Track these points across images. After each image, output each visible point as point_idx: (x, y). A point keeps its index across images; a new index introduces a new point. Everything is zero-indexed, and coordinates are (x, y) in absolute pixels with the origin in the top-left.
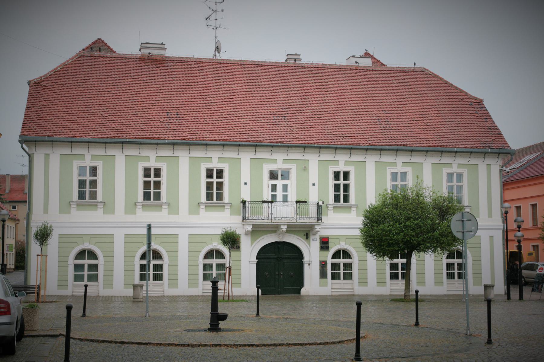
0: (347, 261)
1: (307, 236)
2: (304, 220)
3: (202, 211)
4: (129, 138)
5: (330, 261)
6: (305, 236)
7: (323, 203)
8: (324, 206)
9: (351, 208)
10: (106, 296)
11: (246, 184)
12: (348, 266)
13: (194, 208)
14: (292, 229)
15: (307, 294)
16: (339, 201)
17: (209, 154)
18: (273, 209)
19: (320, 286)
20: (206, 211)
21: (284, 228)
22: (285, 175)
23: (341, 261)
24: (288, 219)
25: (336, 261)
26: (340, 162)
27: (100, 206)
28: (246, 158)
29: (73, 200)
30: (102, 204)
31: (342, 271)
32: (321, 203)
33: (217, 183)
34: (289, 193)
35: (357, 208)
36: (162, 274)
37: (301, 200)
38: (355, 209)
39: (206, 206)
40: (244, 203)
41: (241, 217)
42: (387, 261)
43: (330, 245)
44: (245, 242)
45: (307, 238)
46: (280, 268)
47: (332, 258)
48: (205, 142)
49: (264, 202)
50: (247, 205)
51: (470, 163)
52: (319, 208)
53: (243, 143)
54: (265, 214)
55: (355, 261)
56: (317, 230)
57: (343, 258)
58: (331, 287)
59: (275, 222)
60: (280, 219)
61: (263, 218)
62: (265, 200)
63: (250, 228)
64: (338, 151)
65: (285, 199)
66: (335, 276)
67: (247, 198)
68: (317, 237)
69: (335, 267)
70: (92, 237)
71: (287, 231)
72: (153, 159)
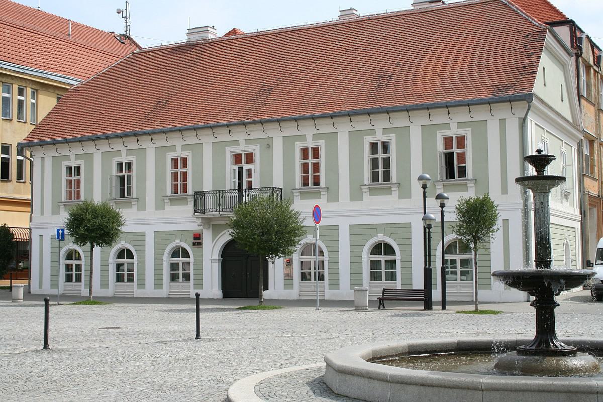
0: (390, 257)
3: (366, 196)
12: (392, 264)
13: (356, 195)
19: (284, 289)
26: (488, 121)
27: (324, 193)
29: (134, 197)
30: (396, 185)
33: (458, 154)
34: (252, 179)
36: (396, 271)
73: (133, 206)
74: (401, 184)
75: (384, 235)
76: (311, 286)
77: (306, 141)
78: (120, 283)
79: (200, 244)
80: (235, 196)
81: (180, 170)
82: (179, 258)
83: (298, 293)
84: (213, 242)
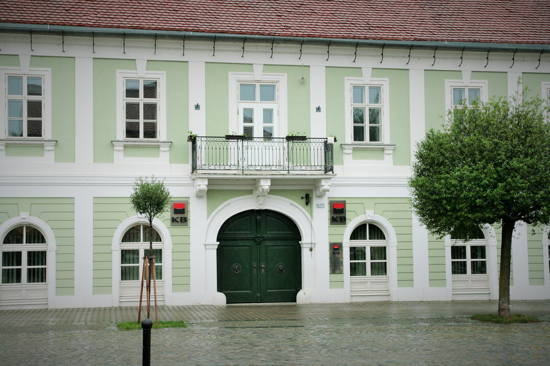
0: (36, 247)
1: (308, 199)
2: (300, 172)
3: (119, 155)
4: (51, 24)
5: (347, 244)
6: (304, 201)
7: (335, 140)
8: (336, 146)
9: (383, 150)
10: (105, 309)
11: (197, 107)
12: (38, 258)
14: (280, 187)
15: (308, 302)
16: (362, 139)
17: (249, 58)
18: (290, 151)
19: (331, 287)
20: (354, 158)
21: (266, 185)
22: (269, 92)
23: (367, 244)
24: (273, 168)
25: (358, 243)
27: (49, 147)
28: (198, 61)
31: (368, 261)
32: (331, 140)
33: (146, 106)
35: (393, 150)
37: (295, 134)
38: (391, 152)
39: (125, 147)
40: (193, 139)
41: (189, 166)
42: (448, 241)
43: (348, 215)
44: (197, 211)
45: (307, 204)
46: (259, 255)
47: (351, 239)
48: (244, 36)
49: (229, 137)
50: (198, 143)
51: (488, 69)
52: (328, 147)
53: (191, 33)
54: (233, 160)
55: (391, 243)
56: (324, 188)
57: (370, 238)
58: (348, 290)
59: (251, 174)
60: (258, 168)
61: (227, 168)
62: (231, 134)
63: (203, 185)
64: (360, 50)
65: (268, 136)
66: (355, 270)
67: (199, 130)
68: (325, 201)
69: (356, 253)
70: (33, 201)
71: (272, 192)
72: (141, 65)
73: (45, 152)
74: (59, 141)
75: (30, 215)
76: (366, 282)
77: (362, 76)
78: (358, 278)
79: (184, 221)
80: (319, 150)
81: (367, 105)
82: (140, 241)
83: (350, 295)
84: (208, 218)
